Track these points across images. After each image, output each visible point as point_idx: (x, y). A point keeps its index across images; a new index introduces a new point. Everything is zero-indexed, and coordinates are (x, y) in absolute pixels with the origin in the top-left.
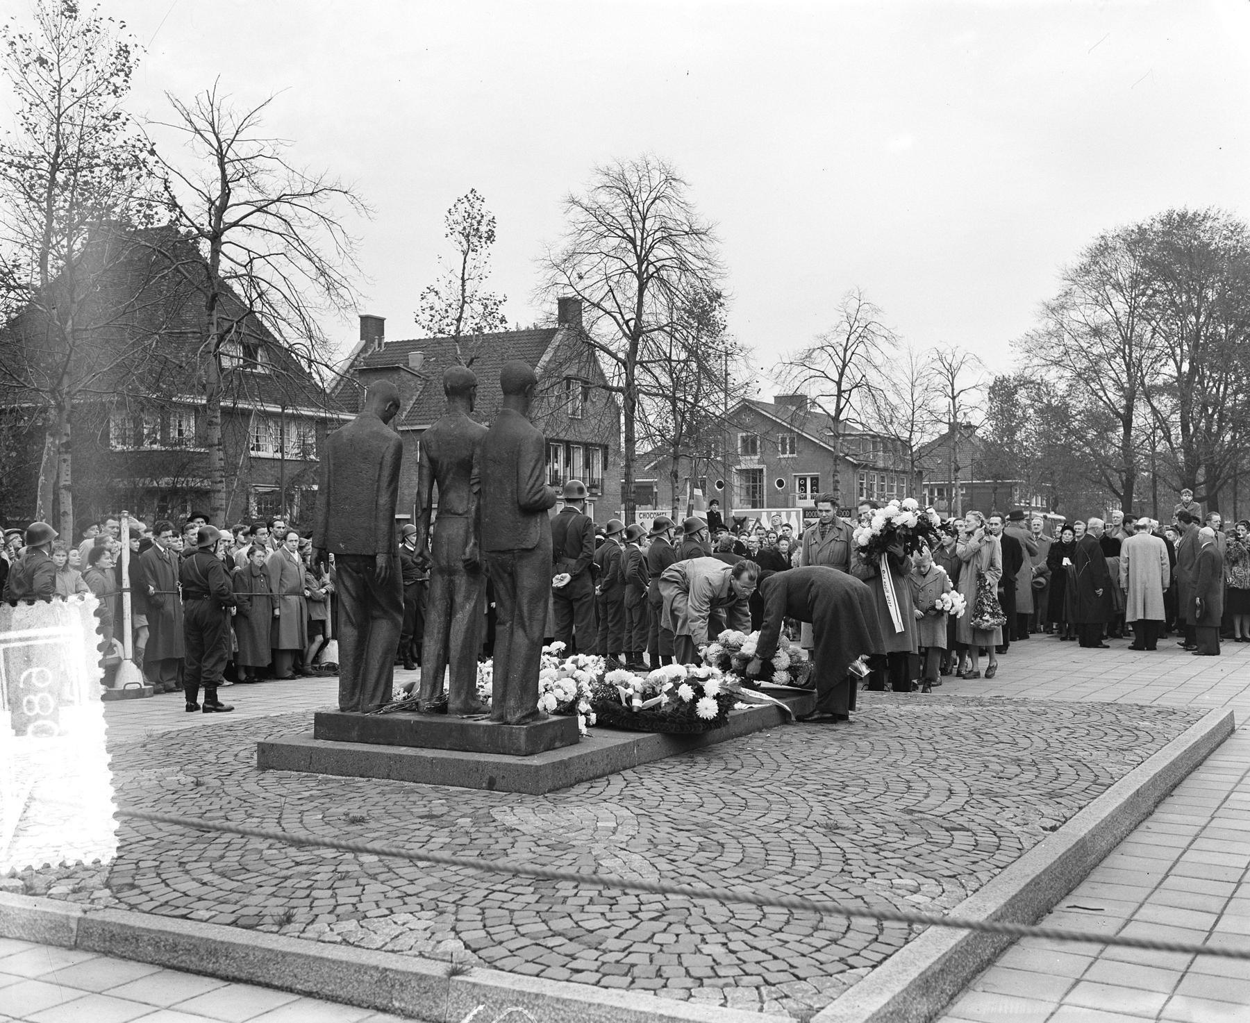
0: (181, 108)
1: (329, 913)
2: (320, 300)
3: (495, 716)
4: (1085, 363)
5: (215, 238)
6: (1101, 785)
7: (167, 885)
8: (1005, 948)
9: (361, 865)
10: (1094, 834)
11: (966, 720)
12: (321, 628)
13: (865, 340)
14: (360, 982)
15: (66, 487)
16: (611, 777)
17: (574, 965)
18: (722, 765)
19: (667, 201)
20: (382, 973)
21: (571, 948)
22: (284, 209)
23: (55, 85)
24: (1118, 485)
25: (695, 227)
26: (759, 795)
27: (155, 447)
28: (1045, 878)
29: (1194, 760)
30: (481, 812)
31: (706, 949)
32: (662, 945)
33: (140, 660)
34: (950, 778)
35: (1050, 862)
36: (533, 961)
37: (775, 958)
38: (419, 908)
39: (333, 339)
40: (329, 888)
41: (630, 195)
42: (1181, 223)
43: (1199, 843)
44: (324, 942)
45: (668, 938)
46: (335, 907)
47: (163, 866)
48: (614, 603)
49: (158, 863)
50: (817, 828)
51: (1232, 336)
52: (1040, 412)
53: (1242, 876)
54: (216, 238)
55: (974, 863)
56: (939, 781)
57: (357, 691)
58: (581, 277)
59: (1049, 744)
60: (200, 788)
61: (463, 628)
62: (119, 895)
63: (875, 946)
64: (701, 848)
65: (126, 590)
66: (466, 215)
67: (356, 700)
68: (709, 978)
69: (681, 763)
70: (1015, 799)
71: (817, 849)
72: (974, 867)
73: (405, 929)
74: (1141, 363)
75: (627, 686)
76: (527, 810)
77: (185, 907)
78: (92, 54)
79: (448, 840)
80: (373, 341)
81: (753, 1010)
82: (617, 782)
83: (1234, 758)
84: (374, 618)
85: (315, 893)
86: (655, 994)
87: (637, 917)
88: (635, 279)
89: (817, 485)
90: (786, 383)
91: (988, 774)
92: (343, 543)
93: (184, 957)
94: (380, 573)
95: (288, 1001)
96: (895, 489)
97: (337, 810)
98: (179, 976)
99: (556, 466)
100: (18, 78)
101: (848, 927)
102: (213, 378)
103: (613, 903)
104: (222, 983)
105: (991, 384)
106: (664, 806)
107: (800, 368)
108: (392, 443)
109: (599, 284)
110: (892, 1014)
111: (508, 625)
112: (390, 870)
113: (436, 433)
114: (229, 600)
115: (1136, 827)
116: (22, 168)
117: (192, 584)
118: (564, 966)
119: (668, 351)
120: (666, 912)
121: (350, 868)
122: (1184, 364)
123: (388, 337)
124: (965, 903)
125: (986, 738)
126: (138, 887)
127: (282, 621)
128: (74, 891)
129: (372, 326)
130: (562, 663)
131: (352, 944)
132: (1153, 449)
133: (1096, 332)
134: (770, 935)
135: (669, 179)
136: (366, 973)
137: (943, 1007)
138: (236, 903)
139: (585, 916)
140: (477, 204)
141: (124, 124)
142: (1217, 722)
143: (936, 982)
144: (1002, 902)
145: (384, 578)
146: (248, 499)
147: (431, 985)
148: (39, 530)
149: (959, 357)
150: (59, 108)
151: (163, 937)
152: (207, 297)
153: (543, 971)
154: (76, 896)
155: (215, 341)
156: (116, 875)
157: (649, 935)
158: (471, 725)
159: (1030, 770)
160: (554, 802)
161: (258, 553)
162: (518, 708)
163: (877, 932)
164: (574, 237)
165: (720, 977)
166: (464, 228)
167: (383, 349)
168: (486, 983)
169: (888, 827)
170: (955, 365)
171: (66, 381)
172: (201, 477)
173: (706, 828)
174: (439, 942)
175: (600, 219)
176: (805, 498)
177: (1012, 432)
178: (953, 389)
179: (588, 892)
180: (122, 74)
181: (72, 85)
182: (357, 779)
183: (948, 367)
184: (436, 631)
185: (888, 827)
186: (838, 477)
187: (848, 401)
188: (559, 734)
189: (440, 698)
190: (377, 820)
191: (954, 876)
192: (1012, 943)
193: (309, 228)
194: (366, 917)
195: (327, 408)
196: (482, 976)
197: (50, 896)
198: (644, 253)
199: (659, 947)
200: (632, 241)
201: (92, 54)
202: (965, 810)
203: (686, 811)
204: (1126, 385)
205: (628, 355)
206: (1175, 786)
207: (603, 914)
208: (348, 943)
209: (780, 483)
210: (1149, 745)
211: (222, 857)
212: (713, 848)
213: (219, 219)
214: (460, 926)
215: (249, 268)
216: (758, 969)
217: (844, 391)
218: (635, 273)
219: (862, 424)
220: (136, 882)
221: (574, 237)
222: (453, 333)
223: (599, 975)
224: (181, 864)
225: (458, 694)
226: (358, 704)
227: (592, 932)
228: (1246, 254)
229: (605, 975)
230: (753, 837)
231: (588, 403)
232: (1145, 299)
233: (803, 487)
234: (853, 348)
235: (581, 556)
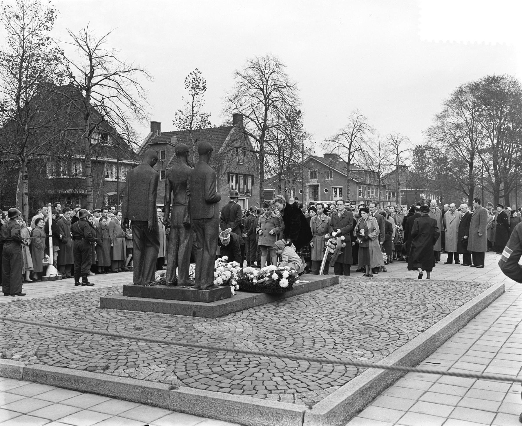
0: (73, 36)
1: (124, 365)
2: (132, 116)
3: (196, 286)
4: (453, 140)
5: (88, 90)
6: (444, 314)
7: (60, 355)
8: (398, 379)
9: (139, 346)
10: (439, 334)
11: (393, 288)
12: (131, 251)
13: (360, 131)
15: (26, 194)
16: (244, 311)
17: (221, 385)
18: (290, 306)
19: (277, 74)
20: (143, 388)
21: (220, 378)
22: (116, 78)
23: (22, 26)
24: (467, 191)
25: (289, 84)
26: (304, 318)
27: (65, 176)
28: (417, 351)
29: (486, 304)
30: (189, 325)
31: (274, 379)
32: (256, 377)
33: (56, 264)
34: (383, 311)
35: (419, 344)
36: (204, 384)
37: (302, 382)
38: (160, 363)
39: (137, 132)
40: (125, 356)
42: (493, 81)
43: (483, 337)
44: (121, 377)
45: (259, 375)
46: (127, 363)
47: (59, 347)
48: (252, 240)
49: (57, 346)
50: (325, 331)
51: (515, 128)
52: (435, 160)
53: (499, 350)
54: (88, 90)
55: (388, 345)
56: (379, 312)
57: (141, 276)
58: (241, 105)
59: (425, 298)
60: (76, 316)
61: (184, 251)
62: (40, 359)
63: (343, 378)
64: (277, 339)
65: (50, 236)
66: (193, 80)
67: (140, 280)
68: (274, 390)
69: (273, 305)
70: (408, 319)
71: (324, 339)
72: (387, 347)
73: (154, 371)
74: (476, 140)
75: (252, 274)
76: (208, 324)
77: (66, 363)
78: (37, 13)
79: (175, 336)
80: (156, 132)
81: (291, 402)
82: (246, 313)
83: (502, 303)
84: (148, 247)
85: (119, 358)
86: (252, 397)
87: (248, 366)
89: (341, 191)
90: (328, 149)
91: (399, 309)
92: (135, 216)
93: (65, 383)
94: (150, 228)
95: (105, 400)
96: (374, 193)
97: (131, 325)
99: (232, 184)
101: (333, 370)
102: (87, 148)
103: (239, 360)
104: (80, 393)
105: (414, 149)
106: (264, 322)
107: (333, 143)
108: (154, 175)
109: (249, 108)
110: (347, 404)
111: (201, 249)
112: (150, 348)
113: (172, 171)
114: (92, 240)
115: (458, 331)
116: (8, 61)
117: (77, 233)
118: (216, 386)
119: (277, 136)
120: (259, 365)
121: (134, 348)
122: (494, 140)
123: (163, 130)
124: (382, 361)
125: (400, 295)
126: (48, 355)
127: (114, 248)
128: (22, 357)
129: (155, 126)
130: (226, 265)
131: (133, 378)
132: (482, 176)
133: (458, 127)
134: (301, 373)
135: (278, 64)
136: (137, 389)
137: (370, 402)
138: (87, 361)
139: (227, 366)
140: (198, 75)
141: (51, 42)
142: (497, 288)
143: (367, 392)
144: (397, 360)
145: (151, 230)
146: (104, 198)
147: (163, 393)
148: (13, 211)
150: (24, 36)
151: (57, 375)
152: (85, 114)
153: (208, 388)
154: (23, 359)
155: (88, 133)
156: (39, 351)
157: (252, 373)
158: (187, 290)
159: (416, 308)
160: (219, 321)
161: (104, 220)
162: (206, 283)
163: (345, 372)
164: (238, 89)
165: (279, 390)
166: (193, 85)
167: (160, 135)
168: (185, 392)
169: (355, 331)
170: (398, 141)
171: (25, 150)
172: (84, 189)
173: (280, 331)
174: (167, 377)
175: (249, 81)
176: (337, 197)
177: (423, 169)
178: (397, 151)
179: (230, 356)
180: (50, 22)
181: (29, 26)
182: (140, 312)
183: (395, 142)
184: (172, 252)
185: (355, 331)
186: (349, 188)
187: (353, 156)
188: (223, 294)
189: (174, 279)
190: (146, 328)
191: (379, 350)
192: (401, 377)
193: (127, 85)
194: (139, 367)
195: (135, 159)
196: (183, 390)
197: (12, 359)
198: (267, 95)
199: (255, 378)
200: (262, 90)
201: (37, 13)
202: (387, 324)
203: (272, 324)
204: (471, 149)
205: (260, 138)
206: (477, 314)
207: (234, 365)
208: (131, 377)
209: (326, 191)
210: (467, 298)
211: (83, 343)
212: (282, 339)
213: (90, 82)
214: (176, 370)
215: (102, 102)
216: (294, 387)
217: (352, 152)
218: (263, 103)
219: (359, 166)
220: (47, 353)
221: (238, 89)
222: (189, 129)
223: (230, 389)
224: (66, 346)
225: (182, 278)
226: (141, 282)
227: (229, 372)
228: (520, 94)
229: (232, 389)
230: (299, 335)
231: (246, 157)
232: (478, 113)
235: (236, 221)
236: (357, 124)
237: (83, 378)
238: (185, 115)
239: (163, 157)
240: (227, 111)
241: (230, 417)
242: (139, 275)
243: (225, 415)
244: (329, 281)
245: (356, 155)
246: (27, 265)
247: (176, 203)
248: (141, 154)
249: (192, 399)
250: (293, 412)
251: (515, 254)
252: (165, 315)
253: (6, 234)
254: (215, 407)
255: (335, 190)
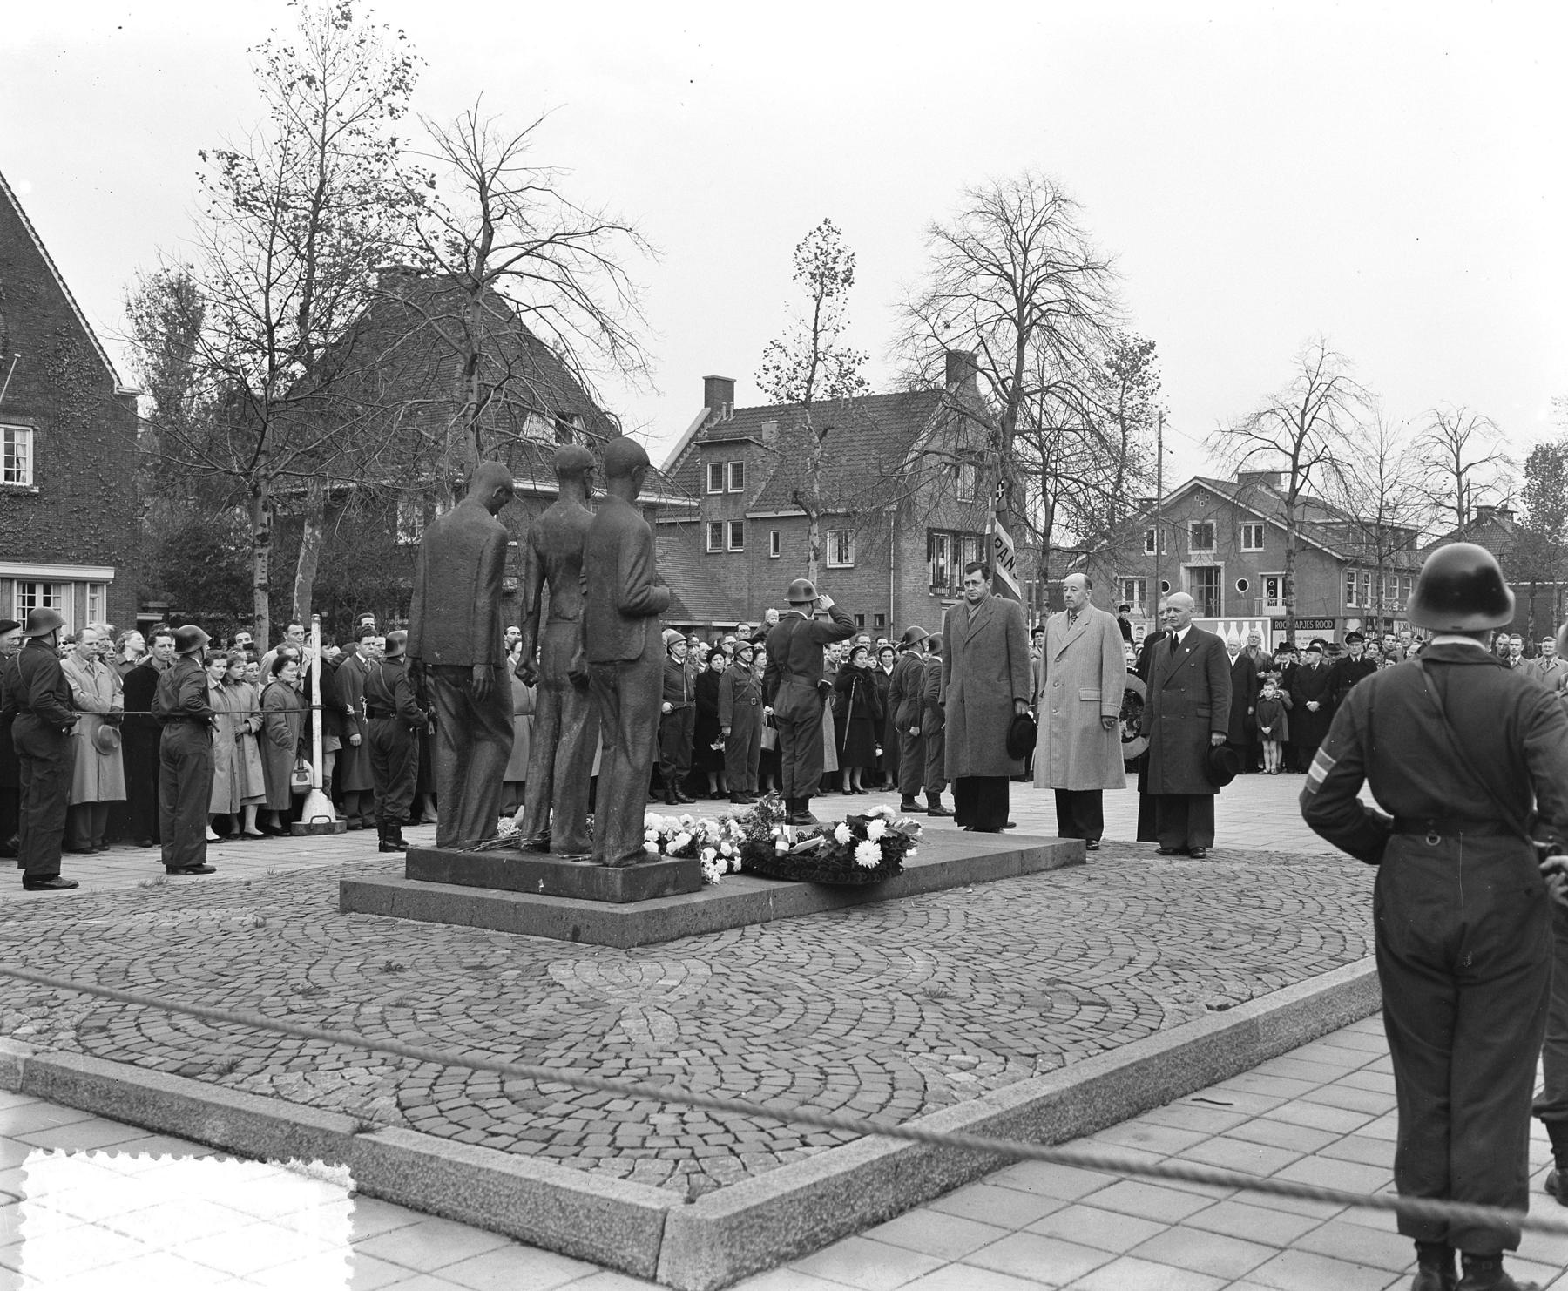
10: (1274, 1018)
13: (1330, 401)
14: (272, 1137)
22: (560, 252)
33: (328, 790)
41: (1007, 221)
57: (456, 824)
65: (316, 707)
66: (819, 251)
67: (453, 835)
80: (720, 408)
84: (479, 740)
88: (1014, 328)
92: (439, 651)
93: (116, 1105)
94: (476, 688)
98: (109, 1123)
99: (942, 562)
100: (277, 100)
108: (493, 534)
117: (377, 699)
129: (718, 389)
135: (1057, 200)
137: (928, 1199)
140: (832, 238)
145: (483, 693)
149: (1466, 423)
151: (99, 1083)
154: (39, 1037)
158: (566, 866)
166: (818, 267)
170: (1461, 431)
174: (373, 1099)
176: (1275, 604)
181: (338, 107)
183: (1451, 433)
184: (540, 756)
187: (1306, 477)
188: (671, 879)
200: (1011, 279)
209: (1243, 585)
217: (1302, 467)
218: (1013, 319)
221: (934, 277)
222: (803, 397)
226: (457, 838)
227: (545, 1094)
233: (1272, 590)
234: (1314, 411)
236: (1319, 380)
237: (159, 1092)
238: (793, 356)
239: (738, 482)
240: (903, 343)
241: (487, 1216)
242: (452, 821)
243: (476, 1210)
244: (1050, 856)
245: (1316, 472)
246: (247, 790)
247: (556, 616)
248: (675, 471)
249: (401, 1163)
250: (638, 1207)
251: (1341, 771)
252: (495, 936)
253: (168, 699)
254: (454, 1185)
255: (1271, 583)
